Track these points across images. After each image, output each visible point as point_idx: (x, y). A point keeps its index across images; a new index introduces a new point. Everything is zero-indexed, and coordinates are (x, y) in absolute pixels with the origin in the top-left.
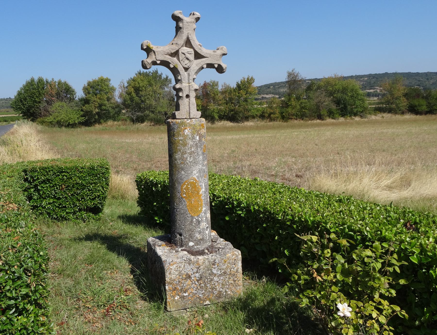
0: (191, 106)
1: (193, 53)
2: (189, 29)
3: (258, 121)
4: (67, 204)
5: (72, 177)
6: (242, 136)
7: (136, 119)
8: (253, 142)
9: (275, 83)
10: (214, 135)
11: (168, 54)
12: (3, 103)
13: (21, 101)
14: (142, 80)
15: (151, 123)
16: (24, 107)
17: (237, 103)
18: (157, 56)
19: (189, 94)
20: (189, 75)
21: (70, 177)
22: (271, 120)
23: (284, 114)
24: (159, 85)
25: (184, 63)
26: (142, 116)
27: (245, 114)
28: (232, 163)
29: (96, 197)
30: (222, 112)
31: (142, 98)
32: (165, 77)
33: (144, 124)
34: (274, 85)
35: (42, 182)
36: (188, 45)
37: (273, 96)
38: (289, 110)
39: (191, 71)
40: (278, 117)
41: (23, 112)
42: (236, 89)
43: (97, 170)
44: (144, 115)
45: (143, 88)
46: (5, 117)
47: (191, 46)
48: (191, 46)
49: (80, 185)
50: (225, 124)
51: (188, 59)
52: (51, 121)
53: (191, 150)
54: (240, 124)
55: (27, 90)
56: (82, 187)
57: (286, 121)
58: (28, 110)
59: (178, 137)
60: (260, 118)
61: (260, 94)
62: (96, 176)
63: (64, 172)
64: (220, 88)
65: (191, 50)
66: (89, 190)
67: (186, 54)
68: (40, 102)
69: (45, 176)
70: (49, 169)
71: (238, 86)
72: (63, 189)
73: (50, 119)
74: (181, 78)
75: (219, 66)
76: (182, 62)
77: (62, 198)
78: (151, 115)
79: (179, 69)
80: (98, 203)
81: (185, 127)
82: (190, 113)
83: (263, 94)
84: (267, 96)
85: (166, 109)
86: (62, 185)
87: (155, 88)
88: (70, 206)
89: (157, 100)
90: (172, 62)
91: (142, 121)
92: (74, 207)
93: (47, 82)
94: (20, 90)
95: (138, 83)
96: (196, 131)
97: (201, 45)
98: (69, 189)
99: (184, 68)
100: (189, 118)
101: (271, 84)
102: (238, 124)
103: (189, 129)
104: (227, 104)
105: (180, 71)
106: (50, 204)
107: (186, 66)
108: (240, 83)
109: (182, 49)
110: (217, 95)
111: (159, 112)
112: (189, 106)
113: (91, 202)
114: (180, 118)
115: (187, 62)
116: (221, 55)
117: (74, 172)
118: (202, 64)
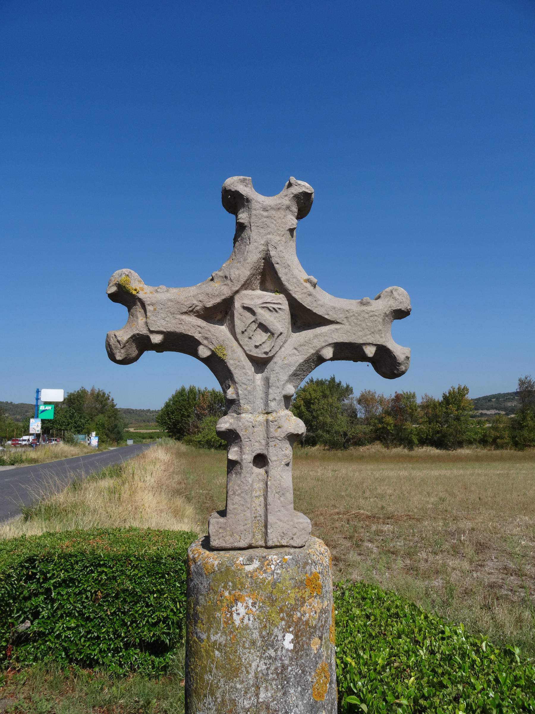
0: (270, 499)
1: (285, 306)
2: (269, 230)
3: (477, 448)
4: (103, 633)
5: (116, 577)
6: (455, 471)
7: (305, 440)
8: (473, 484)
9: (499, 394)
10: (412, 468)
11: (191, 311)
12: (153, 415)
13: (168, 414)
14: (314, 390)
15: (325, 446)
16: (170, 421)
17: (445, 422)
18: (152, 318)
19: (265, 452)
20: (267, 381)
21: (113, 576)
22: (498, 447)
23: (517, 439)
24: (336, 396)
25: (253, 343)
26: (313, 437)
27: (458, 438)
28: (441, 524)
29: (160, 620)
30: (423, 434)
31: (314, 414)
32: (345, 386)
33: (316, 447)
34: (498, 397)
35: (60, 585)
36: (269, 285)
37: (496, 412)
38: (525, 433)
39: (277, 368)
40: (507, 444)
41: (169, 427)
42: (442, 402)
43: (165, 565)
44: (317, 436)
45: (316, 400)
46: (152, 433)
47: (280, 288)
48: (280, 288)
49: (130, 594)
50: (428, 450)
51: (263, 327)
52: (199, 440)
53: (257, 695)
54: (450, 452)
55: (176, 401)
56: (133, 597)
57: (522, 449)
58: (175, 424)
59: (209, 629)
60: (480, 443)
61: (478, 410)
62: (163, 577)
63: (104, 565)
64: (419, 401)
65: (281, 298)
66: (147, 606)
67: (259, 311)
68: (189, 416)
69: (67, 571)
70: (76, 557)
71: (445, 398)
72: (98, 599)
73: (198, 437)
74: (237, 394)
75: (382, 350)
76: (243, 339)
77: (95, 618)
78: (325, 436)
79: (231, 363)
80: (164, 633)
81: (237, 593)
82: (266, 527)
83: (482, 410)
84: (488, 412)
85: (345, 429)
86: (95, 592)
87: (331, 401)
88: (108, 636)
89: (333, 416)
90: (206, 338)
91: (314, 444)
92: (116, 639)
93: (199, 391)
94: (168, 401)
95: (310, 394)
96: (281, 610)
97: (315, 280)
98: (108, 601)
99: (251, 358)
100: (262, 543)
101: (493, 396)
102: (447, 452)
103: (250, 602)
104: (430, 423)
105: (232, 368)
106: (69, 629)
107: (259, 353)
108: (448, 395)
109: (246, 296)
110: (416, 410)
111: (336, 432)
112: (266, 499)
113: (150, 631)
114: (228, 546)
115: (260, 337)
116: (386, 315)
117: (122, 566)
118: (318, 344)
